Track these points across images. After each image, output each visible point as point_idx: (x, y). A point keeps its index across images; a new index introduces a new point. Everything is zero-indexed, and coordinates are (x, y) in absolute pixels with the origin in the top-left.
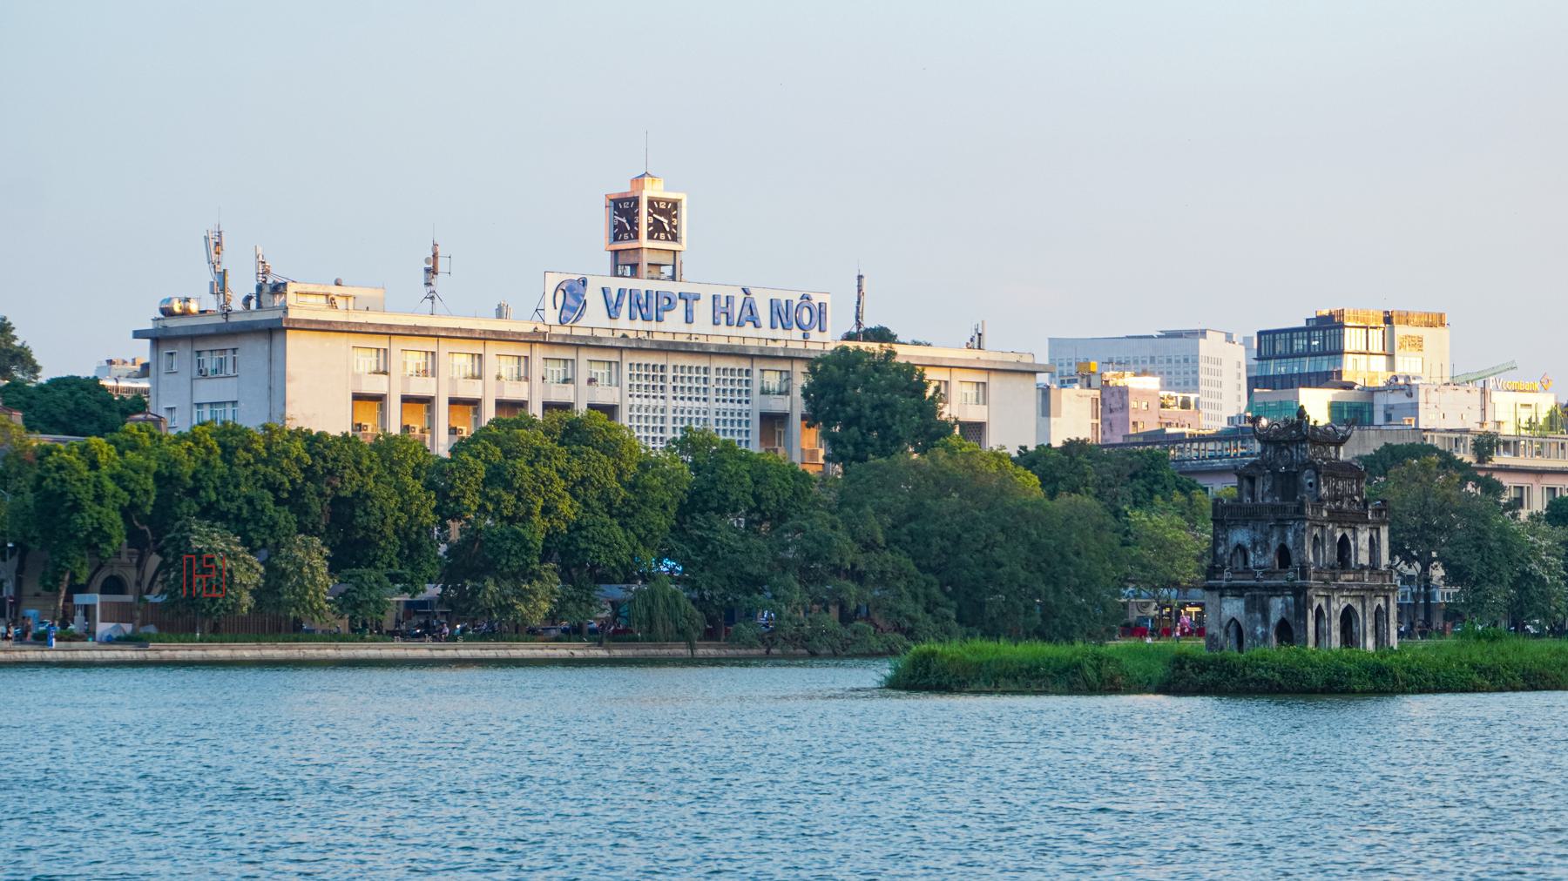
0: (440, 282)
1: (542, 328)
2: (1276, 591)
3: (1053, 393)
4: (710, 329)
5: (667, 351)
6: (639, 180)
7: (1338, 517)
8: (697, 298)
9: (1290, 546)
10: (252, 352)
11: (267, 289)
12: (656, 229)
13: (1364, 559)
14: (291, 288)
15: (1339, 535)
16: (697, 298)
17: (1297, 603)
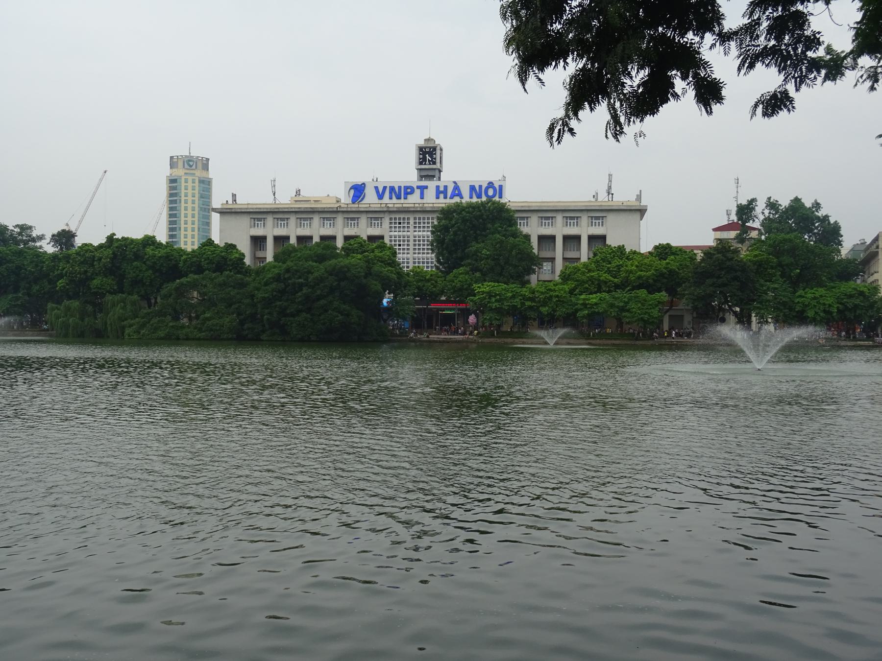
8: (426, 187)
16: (426, 187)
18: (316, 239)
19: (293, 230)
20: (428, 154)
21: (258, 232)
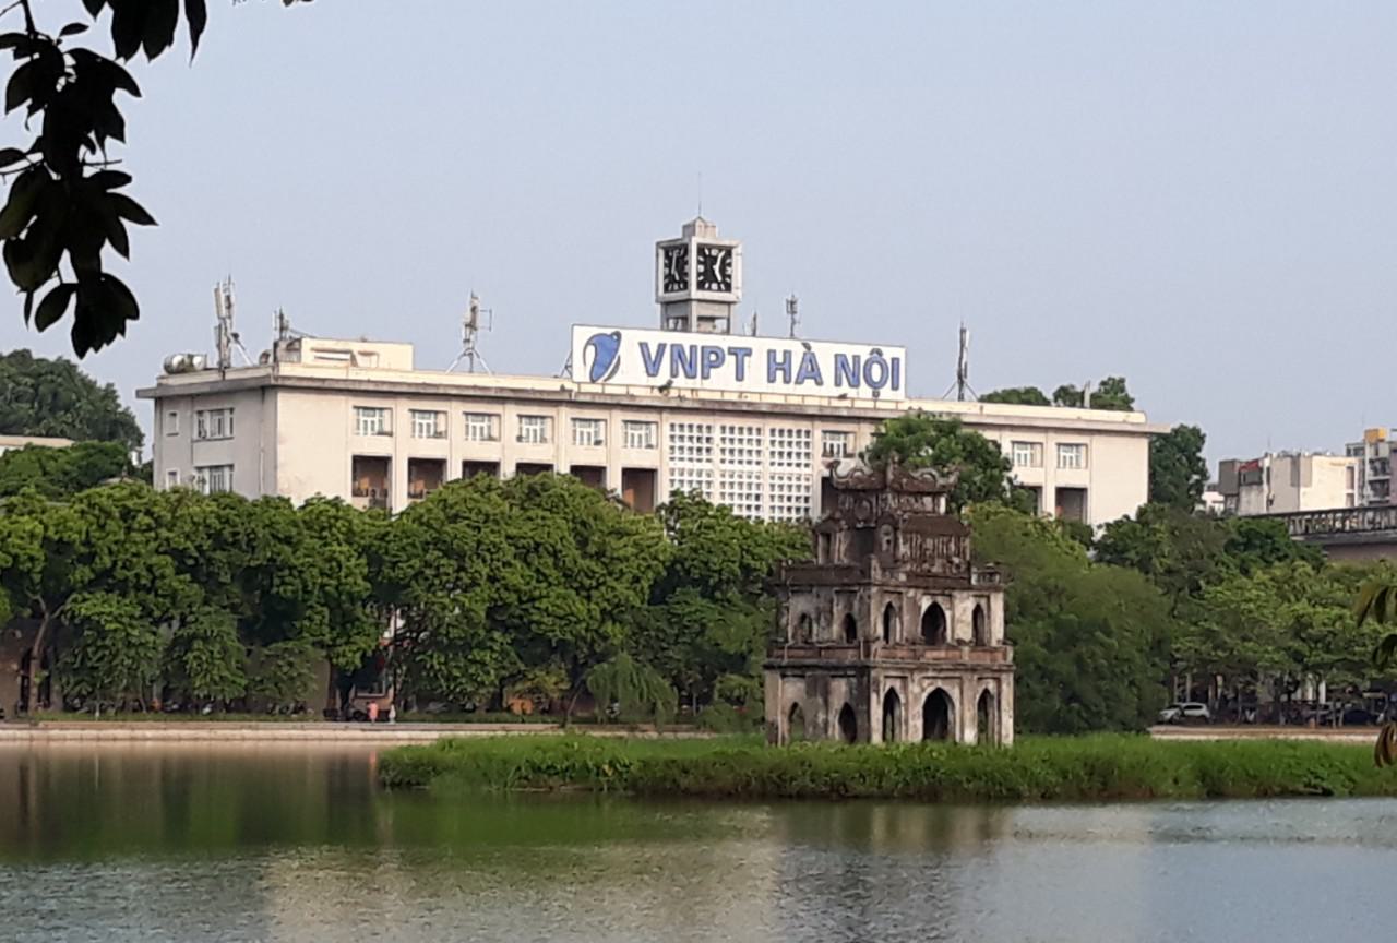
0: (481, 338)
1: (568, 385)
2: (838, 670)
3: (1302, 460)
4: (765, 386)
5: (712, 412)
6: (689, 229)
7: (922, 581)
8: (748, 352)
9: (856, 617)
10: (245, 410)
11: (283, 345)
12: (707, 278)
13: (965, 632)
14: (307, 344)
15: (925, 603)
16: (748, 352)
17: (860, 683)
18: (508, 471)
19: (458, 444)
20: (690, 272)
21: (375, 447)
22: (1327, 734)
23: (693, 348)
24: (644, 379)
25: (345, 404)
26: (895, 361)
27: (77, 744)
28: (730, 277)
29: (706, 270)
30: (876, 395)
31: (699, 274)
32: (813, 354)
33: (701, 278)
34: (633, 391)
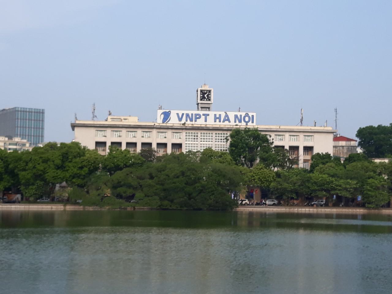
4: (213, 123)
8: (208, 115)
22: (356, 209)
23: (192, 114)
24: (178, 122)
25: (93, 130)
26: (253, 116)
27: (14, 209)
28: (210, 97)
29: (203, 96)
30: (247, 124)
31: (201, 97)
32: (228, 115)
33: (201, 98)
34: (174, 125)
